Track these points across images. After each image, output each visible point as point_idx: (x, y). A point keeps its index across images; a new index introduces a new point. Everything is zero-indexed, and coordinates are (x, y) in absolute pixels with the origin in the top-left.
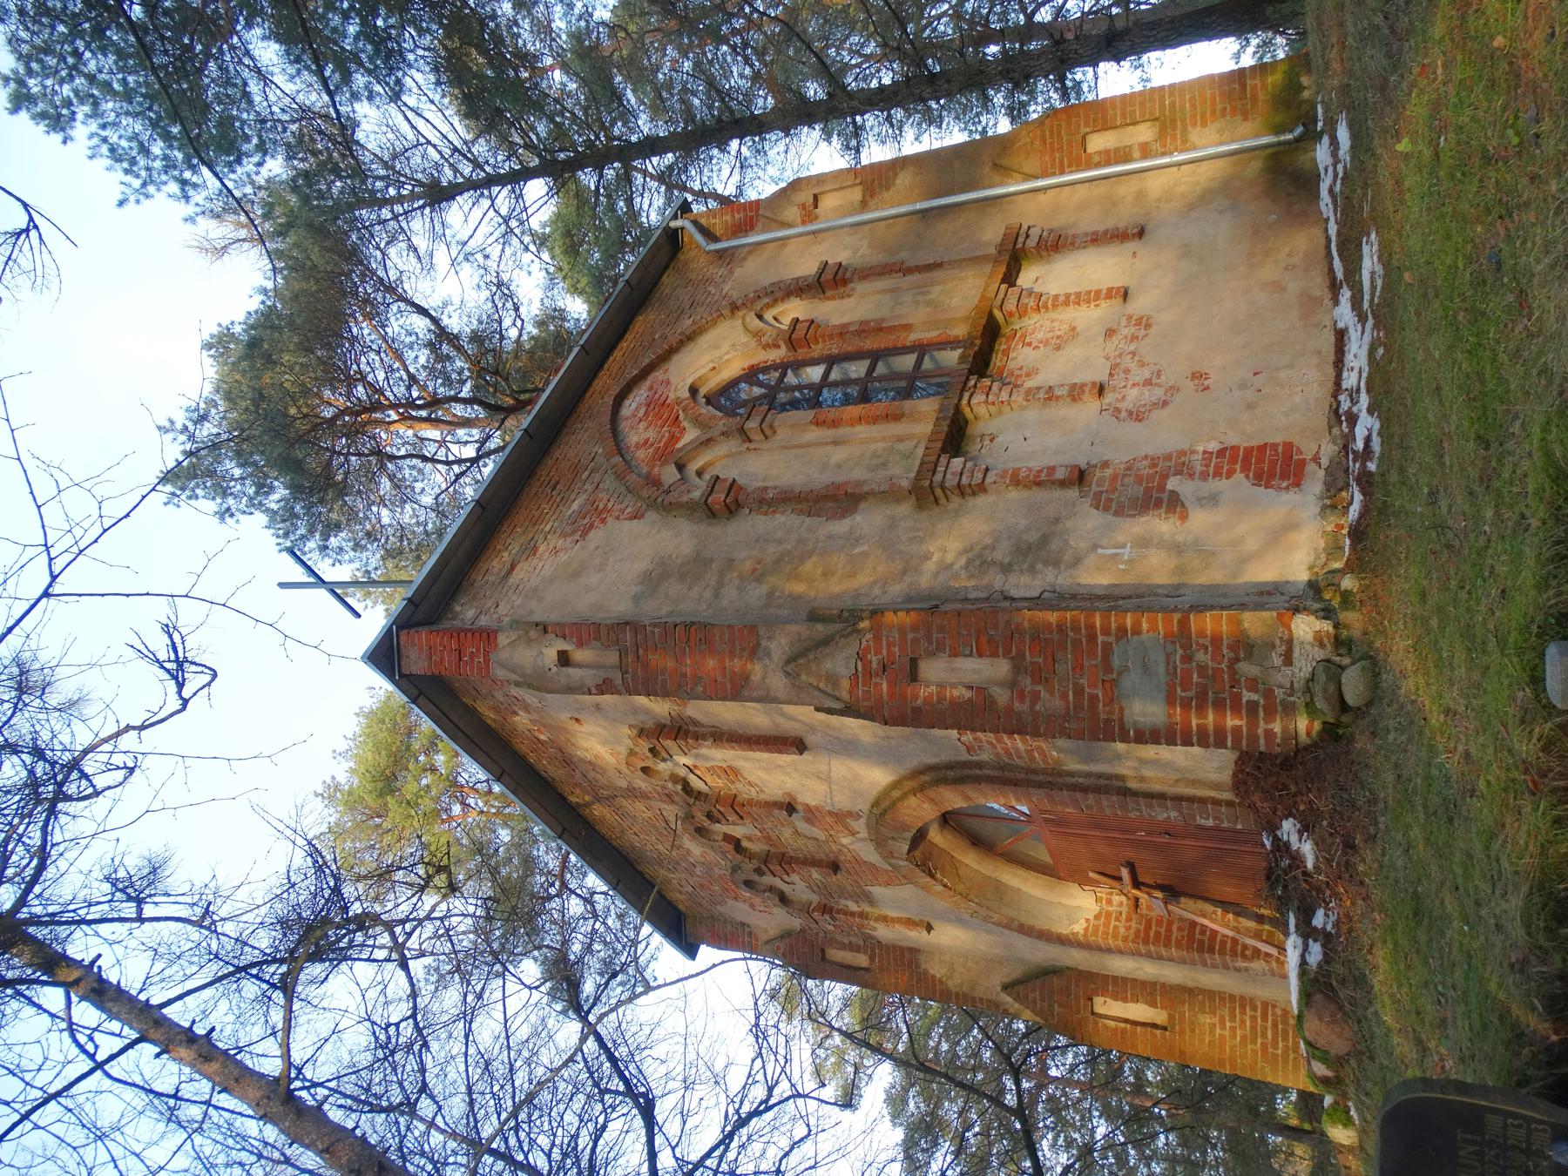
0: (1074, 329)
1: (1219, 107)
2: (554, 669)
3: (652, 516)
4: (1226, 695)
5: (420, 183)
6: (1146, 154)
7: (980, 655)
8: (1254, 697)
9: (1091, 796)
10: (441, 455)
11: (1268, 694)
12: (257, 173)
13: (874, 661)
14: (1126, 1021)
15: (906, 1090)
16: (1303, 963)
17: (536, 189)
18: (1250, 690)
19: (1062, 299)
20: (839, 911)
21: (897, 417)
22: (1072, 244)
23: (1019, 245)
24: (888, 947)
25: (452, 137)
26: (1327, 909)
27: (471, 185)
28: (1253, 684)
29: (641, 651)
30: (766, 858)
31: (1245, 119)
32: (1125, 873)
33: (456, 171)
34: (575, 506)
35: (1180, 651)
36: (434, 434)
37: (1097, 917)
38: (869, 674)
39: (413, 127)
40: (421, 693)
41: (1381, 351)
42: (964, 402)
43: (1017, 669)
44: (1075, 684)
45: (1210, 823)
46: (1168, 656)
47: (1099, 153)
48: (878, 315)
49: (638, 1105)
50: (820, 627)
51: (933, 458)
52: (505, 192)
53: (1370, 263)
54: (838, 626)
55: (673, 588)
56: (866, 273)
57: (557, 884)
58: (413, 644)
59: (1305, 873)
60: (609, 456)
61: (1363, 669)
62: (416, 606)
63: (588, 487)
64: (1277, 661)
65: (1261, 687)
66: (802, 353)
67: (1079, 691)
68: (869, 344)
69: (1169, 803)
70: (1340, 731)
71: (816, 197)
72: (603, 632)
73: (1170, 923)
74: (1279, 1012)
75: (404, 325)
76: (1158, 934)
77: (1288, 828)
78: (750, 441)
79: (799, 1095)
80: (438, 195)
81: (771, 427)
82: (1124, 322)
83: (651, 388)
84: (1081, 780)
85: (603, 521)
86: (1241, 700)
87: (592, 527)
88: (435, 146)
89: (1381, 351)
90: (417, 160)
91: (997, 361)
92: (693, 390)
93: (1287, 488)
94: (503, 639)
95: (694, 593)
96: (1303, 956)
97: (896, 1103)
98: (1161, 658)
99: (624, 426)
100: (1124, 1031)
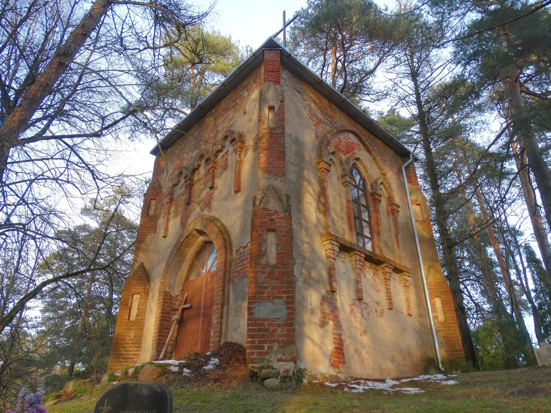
0: (379, 291)
1: (450, 343)
2: (268, 104)
3: (317, 142)
4: (266, 339)
5: (417, 70)
6: (434, 317)
7: (278, 254)
8: (266, 348)
9: (221, 293)
10: (324, 72)
11: (267, 353)
12: (425, 12)
13: (274, 217)
14: (131, 306)
15: (88, 231)
16: (170, 365)
17: (414, 110)
18: (268, 347)
19: (389, 287)
20: (170, 205)
21: (350, 229)
22: (406, 292)
23: (406, 273)
24: (156, 222)
25: (434, 81)
26: (191, 373)
27: (417, 86)
28: (270, 348)
29: (275, 135)
30: (191, 180)
31: (446, 351)
32: (188, 305)
33: (422, 82)
34: (320, 116)
35: (281, 323)
36: (330, 70)
37: (171, 296)
38: (270, 215)
39: (438, 68)
40: (256, 57)
41: (386, 393)
42: (357, 252)
43: (273, 266)
44: (268, 286)
45: (212, 334)
46: (280, 319)
47: (435, 302)
48: (382, 225)
49: (99, 131)
50: (285, 198)
51: (339, 241)
52: (414, 99)
53: (413, 390)
54: (286, 205)
55: (294, 148)
56: (395, 220)
57: (168, 107)
58: (275, 55)
59: (202, 366)
60: (337, 129)
61: (278, 386)
62: (288, 57)
63: (326, 121)
64: (279, 356)
65: (269, 351)
66: (370, 198)
67: (266, 288)
68: (373, 221)
69: (220, 320)
70: (254, 378)
71: (419, 205)
72: (282, 122)
73: (169, 321)
74: (136, 360)
75: (369, 62)
76: (287, 287)
77: (216, 360)
78: (342, 178)
79: (99, 190)
80: (414, 75)
81: (347, 185)
82: (382, 308)
83: (358, 144)
84: (227, 289)
85: (315, 125)
86: (264, 343)
87: (313, 121)
88: (431, 75)
89: (386, 393)
90: (426, 69)
91: (368, 264)
92: (358, 159)
93: (330, 362)
94: (278, 87)
95: (292, 155)
96: (172, 365)
97: (84, 228)
98: (279, 316)
99: (346, 134)
100: (127, 305)
